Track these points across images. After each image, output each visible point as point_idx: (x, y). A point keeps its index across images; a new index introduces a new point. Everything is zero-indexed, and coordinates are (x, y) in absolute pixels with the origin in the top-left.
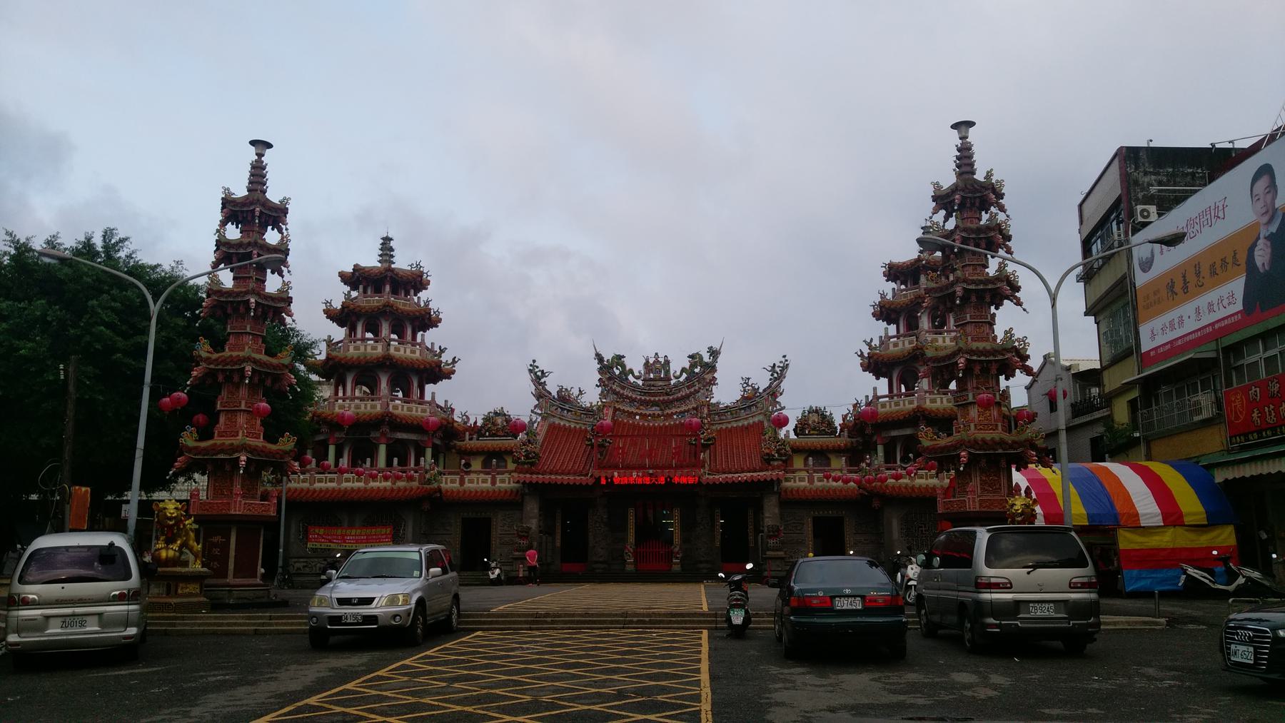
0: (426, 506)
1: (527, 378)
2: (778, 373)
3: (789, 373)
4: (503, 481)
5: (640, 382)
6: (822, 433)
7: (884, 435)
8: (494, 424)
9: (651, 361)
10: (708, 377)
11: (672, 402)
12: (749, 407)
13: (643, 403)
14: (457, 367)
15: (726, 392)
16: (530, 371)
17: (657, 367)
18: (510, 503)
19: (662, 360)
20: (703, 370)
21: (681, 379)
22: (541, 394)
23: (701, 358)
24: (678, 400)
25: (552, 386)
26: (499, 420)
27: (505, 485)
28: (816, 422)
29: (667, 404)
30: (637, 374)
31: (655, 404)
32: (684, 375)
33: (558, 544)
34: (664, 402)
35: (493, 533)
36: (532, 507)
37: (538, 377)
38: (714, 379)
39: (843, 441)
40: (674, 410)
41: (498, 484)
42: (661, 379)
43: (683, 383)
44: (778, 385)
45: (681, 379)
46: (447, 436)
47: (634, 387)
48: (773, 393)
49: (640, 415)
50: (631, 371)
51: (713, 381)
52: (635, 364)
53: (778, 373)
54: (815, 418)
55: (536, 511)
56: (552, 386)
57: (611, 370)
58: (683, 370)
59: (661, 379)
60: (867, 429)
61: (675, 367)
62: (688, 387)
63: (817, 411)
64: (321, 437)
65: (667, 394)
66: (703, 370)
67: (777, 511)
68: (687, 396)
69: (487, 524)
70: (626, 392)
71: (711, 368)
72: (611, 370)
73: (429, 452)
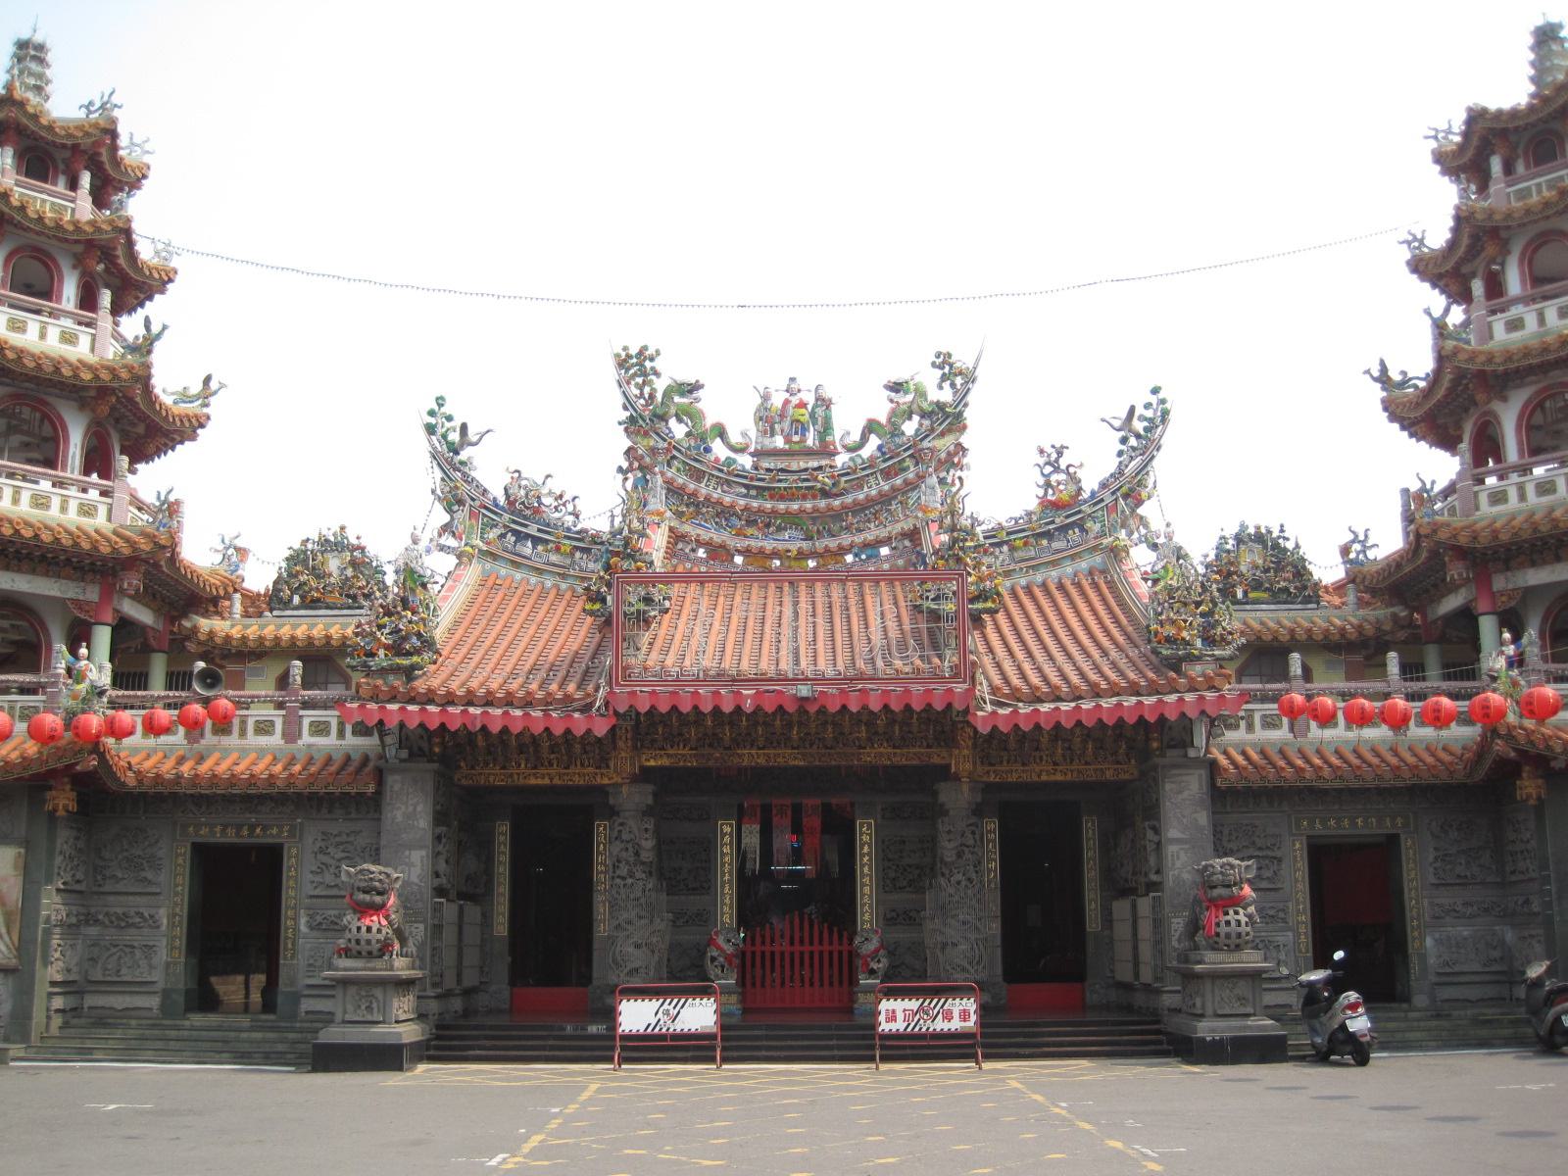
0: (63, 800)
1: (420, 446)
2: (1142, 435)
3: (1171, 438)
4: (320, 729)
5: (746, 461)
6: (1280, 596)
7: (1499, 583)
8: (320, 574)
9: (777, 401)
10: (945, 444)
11: (837, 516)
12: (1064, 529)
13: (752, 519)
14: (216, 408)
15: (996, 490)
16: (430, 429)
17: (797, 421)
18: (342, 800)
19: (810, 399)
20: (929, 431)
21: (868, 451)
22: (458, 493)
23: (921, 393)
24: (858, 508)
25: (491, 473)
26: (333, 564)
27: (329, 741)
28: (1266, 566)
29: (832, 521)
30: (735, 437)
31: (792, 520)
32: (874, 442)
33: (501, 926)
34: (816, 516)
35: (289, 894)
36: (411, 810)
37: (450, 451)
38: (961, 449)
39: (1343, 616)
40: (846, 539)
41: (306, 738)
42: (809, 453)
43: (871, 463)
44: (1143, 469)
45: (868, 451)
46: (154, 604)
47: (728, 476)
48: (1128, 491)
49: (746, 552)
50: (721, 432)
51: (954, 459)
52: (731, 410)
53: (1142, 435)
54: (1249, 560)
55: (424, 823)
56: (491, 473)
57: (656, 422)
58: (871, 427)
59: (809, 453)
60: (1427, 601)
61: (847, 423)
62: (887, 474)
63: (1260, 538)
64: (1451, 603)
65: (825, 494)
66: (929, 431)
67: (1203, 818)
68: (885, 499)
69: (270, 860)
70: (704, 489)
71: (948, 419)
72: (656, 422)
73: (103, 636)
